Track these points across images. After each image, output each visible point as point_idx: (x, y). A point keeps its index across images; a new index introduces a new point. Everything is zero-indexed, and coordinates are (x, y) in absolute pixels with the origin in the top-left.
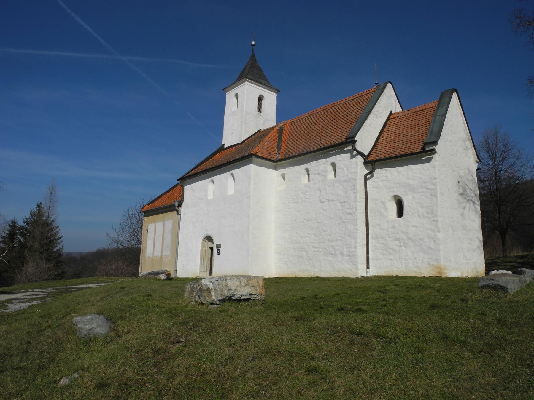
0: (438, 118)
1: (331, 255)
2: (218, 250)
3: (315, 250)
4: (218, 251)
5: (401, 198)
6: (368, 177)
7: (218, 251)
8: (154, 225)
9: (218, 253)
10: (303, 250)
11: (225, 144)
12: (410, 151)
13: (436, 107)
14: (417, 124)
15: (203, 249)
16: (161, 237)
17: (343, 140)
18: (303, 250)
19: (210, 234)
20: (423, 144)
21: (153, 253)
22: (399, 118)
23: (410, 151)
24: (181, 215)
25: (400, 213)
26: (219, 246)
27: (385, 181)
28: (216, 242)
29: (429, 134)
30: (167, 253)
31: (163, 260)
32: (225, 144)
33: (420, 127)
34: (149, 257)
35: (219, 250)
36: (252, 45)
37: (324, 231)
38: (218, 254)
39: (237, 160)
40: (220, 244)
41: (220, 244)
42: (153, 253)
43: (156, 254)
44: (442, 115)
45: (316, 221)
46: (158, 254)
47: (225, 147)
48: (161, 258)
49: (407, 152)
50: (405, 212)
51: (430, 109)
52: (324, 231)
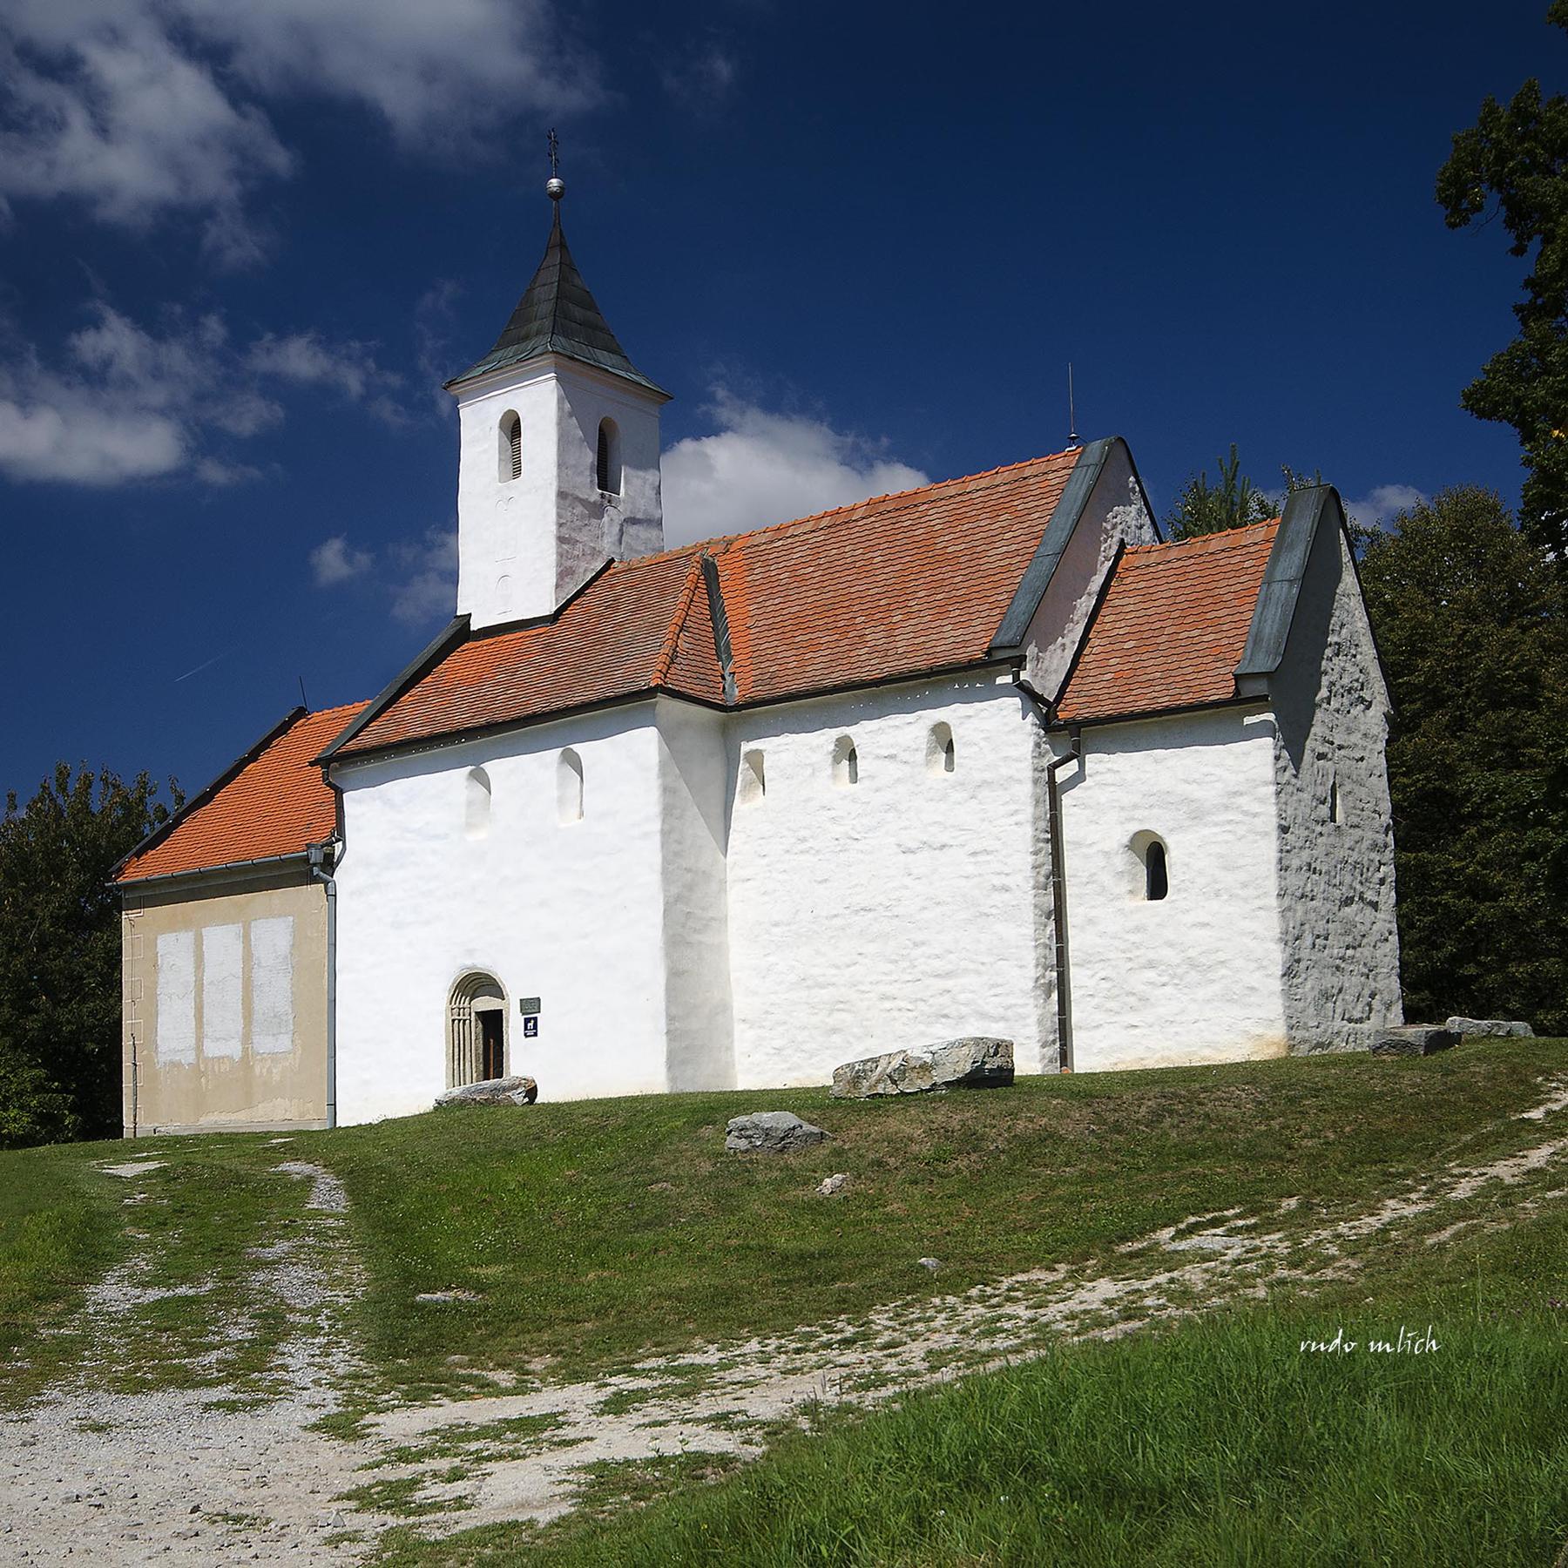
0: (1276, 587)
1: (943, 1020)
2: (527, 1021)
3: (888, 1005)
4: (531, 1024)
5: (1161, 838)
6: (1062, 774)
7: (531, 1024)
8: (187, 938)
9: (531, 1026)
10: (841, 1006)
11: (470, 615)
12: (1191, 695)
13: (1272, 545)
16: (239, 983)
17: (976, 651)
18: (841, 1006)
19: (483, 962)
21: (199, 1047)
22: (1151, 570)
23: (1191, 695)
24: (335, 896)
25: (1157, 888)
26: (531, 1007)
27: (1113, 785)
28: (515, 992)
29: (1250, 645)
30: (275, 1043)
31: (257, 1070)
32: (470, 615)
34: (176, 1065)
35: (535, 1019)
36: (555, 196)
37: (916, 945)
40: (539, 999)
41: (539, 999)
42: (199, 1047)
43: (212, 1049)
45: (887, 914)
46: (224, 1045)
47: (474, 627)
48: (246, 1060)
51: (1252, 549)
52: (916, 945)
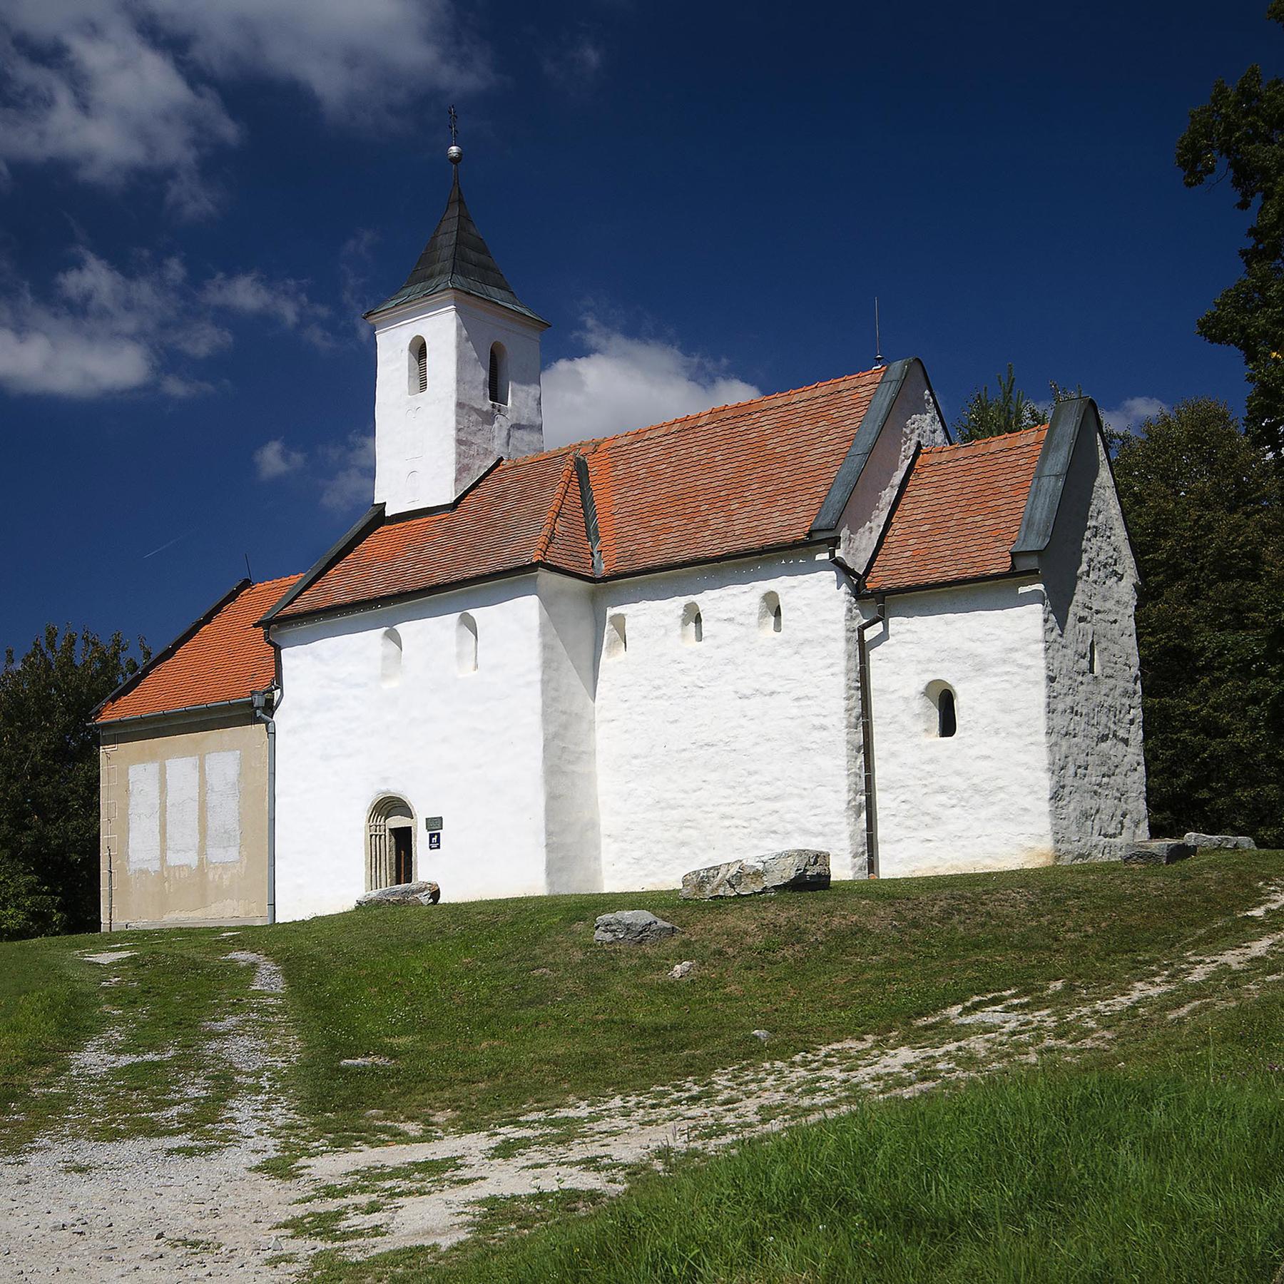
0: (1045, 481)
1: (772, 835)
2: (431, 836)
3: (727, 823)
5: (950, 686)
6: (869, 634)
7: (435, 839)
9: (435, 841)
10: (689, 824)
11: (385, 503)
12: (975, 569)
13: (1041, 446)
14: (991, 491)
15: (374, 837)
16: (196, 805)
18: (689, 824)
19: (396, 788)
20: (1010, 559)
21: (163, 858)
22: (943, 466)
23: (975, 569)
25: (948, 727)
26: (435, 825)
27: (911, 643)
28: (422, 813)
29: (1024, 528)
30: (225, 854)
31: (211, 876)
33: (999, 502)
34: (144, 872)
35: (438, 834)
36: (455, 160)
37: (750, 774)
38: (435, 846)
39: (511, 570)
41: (441, 818)
43: (173, 859)
44: (1056, 475)
45: (726, 748)
46: (184, 856)
47: (388, 514)
48: (202, 868)
49: (969, 571)
50: (959, 722)
52: (750, 774)
